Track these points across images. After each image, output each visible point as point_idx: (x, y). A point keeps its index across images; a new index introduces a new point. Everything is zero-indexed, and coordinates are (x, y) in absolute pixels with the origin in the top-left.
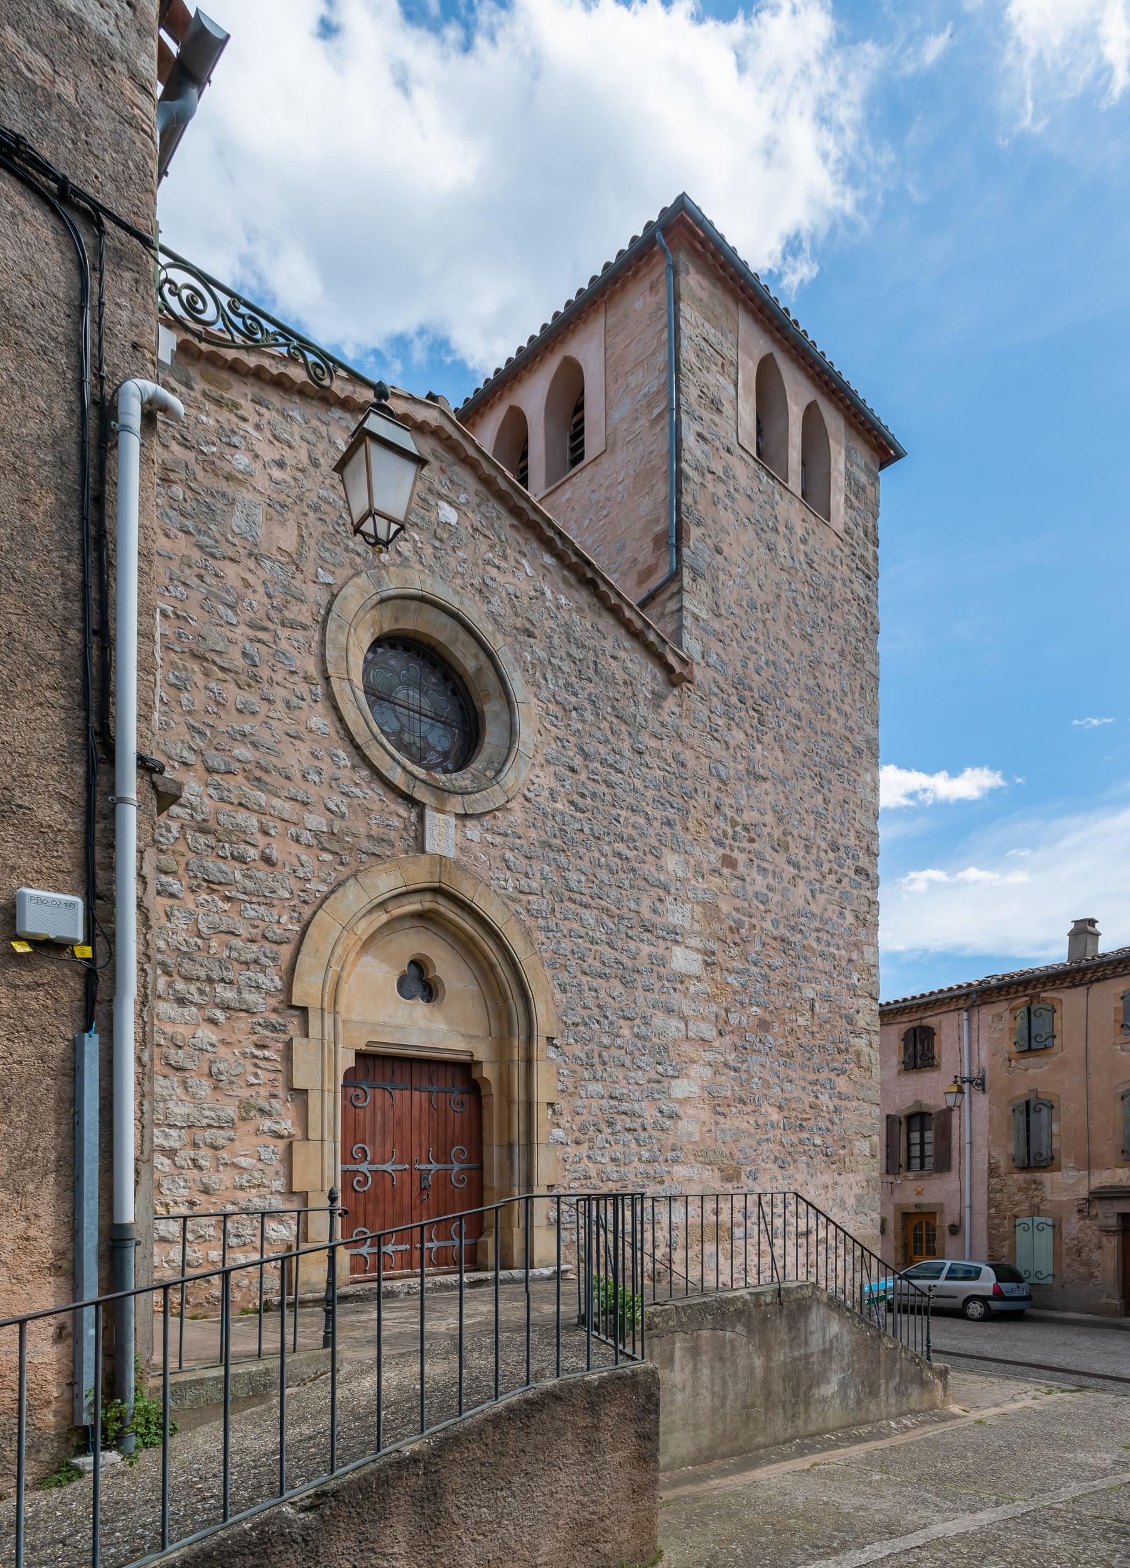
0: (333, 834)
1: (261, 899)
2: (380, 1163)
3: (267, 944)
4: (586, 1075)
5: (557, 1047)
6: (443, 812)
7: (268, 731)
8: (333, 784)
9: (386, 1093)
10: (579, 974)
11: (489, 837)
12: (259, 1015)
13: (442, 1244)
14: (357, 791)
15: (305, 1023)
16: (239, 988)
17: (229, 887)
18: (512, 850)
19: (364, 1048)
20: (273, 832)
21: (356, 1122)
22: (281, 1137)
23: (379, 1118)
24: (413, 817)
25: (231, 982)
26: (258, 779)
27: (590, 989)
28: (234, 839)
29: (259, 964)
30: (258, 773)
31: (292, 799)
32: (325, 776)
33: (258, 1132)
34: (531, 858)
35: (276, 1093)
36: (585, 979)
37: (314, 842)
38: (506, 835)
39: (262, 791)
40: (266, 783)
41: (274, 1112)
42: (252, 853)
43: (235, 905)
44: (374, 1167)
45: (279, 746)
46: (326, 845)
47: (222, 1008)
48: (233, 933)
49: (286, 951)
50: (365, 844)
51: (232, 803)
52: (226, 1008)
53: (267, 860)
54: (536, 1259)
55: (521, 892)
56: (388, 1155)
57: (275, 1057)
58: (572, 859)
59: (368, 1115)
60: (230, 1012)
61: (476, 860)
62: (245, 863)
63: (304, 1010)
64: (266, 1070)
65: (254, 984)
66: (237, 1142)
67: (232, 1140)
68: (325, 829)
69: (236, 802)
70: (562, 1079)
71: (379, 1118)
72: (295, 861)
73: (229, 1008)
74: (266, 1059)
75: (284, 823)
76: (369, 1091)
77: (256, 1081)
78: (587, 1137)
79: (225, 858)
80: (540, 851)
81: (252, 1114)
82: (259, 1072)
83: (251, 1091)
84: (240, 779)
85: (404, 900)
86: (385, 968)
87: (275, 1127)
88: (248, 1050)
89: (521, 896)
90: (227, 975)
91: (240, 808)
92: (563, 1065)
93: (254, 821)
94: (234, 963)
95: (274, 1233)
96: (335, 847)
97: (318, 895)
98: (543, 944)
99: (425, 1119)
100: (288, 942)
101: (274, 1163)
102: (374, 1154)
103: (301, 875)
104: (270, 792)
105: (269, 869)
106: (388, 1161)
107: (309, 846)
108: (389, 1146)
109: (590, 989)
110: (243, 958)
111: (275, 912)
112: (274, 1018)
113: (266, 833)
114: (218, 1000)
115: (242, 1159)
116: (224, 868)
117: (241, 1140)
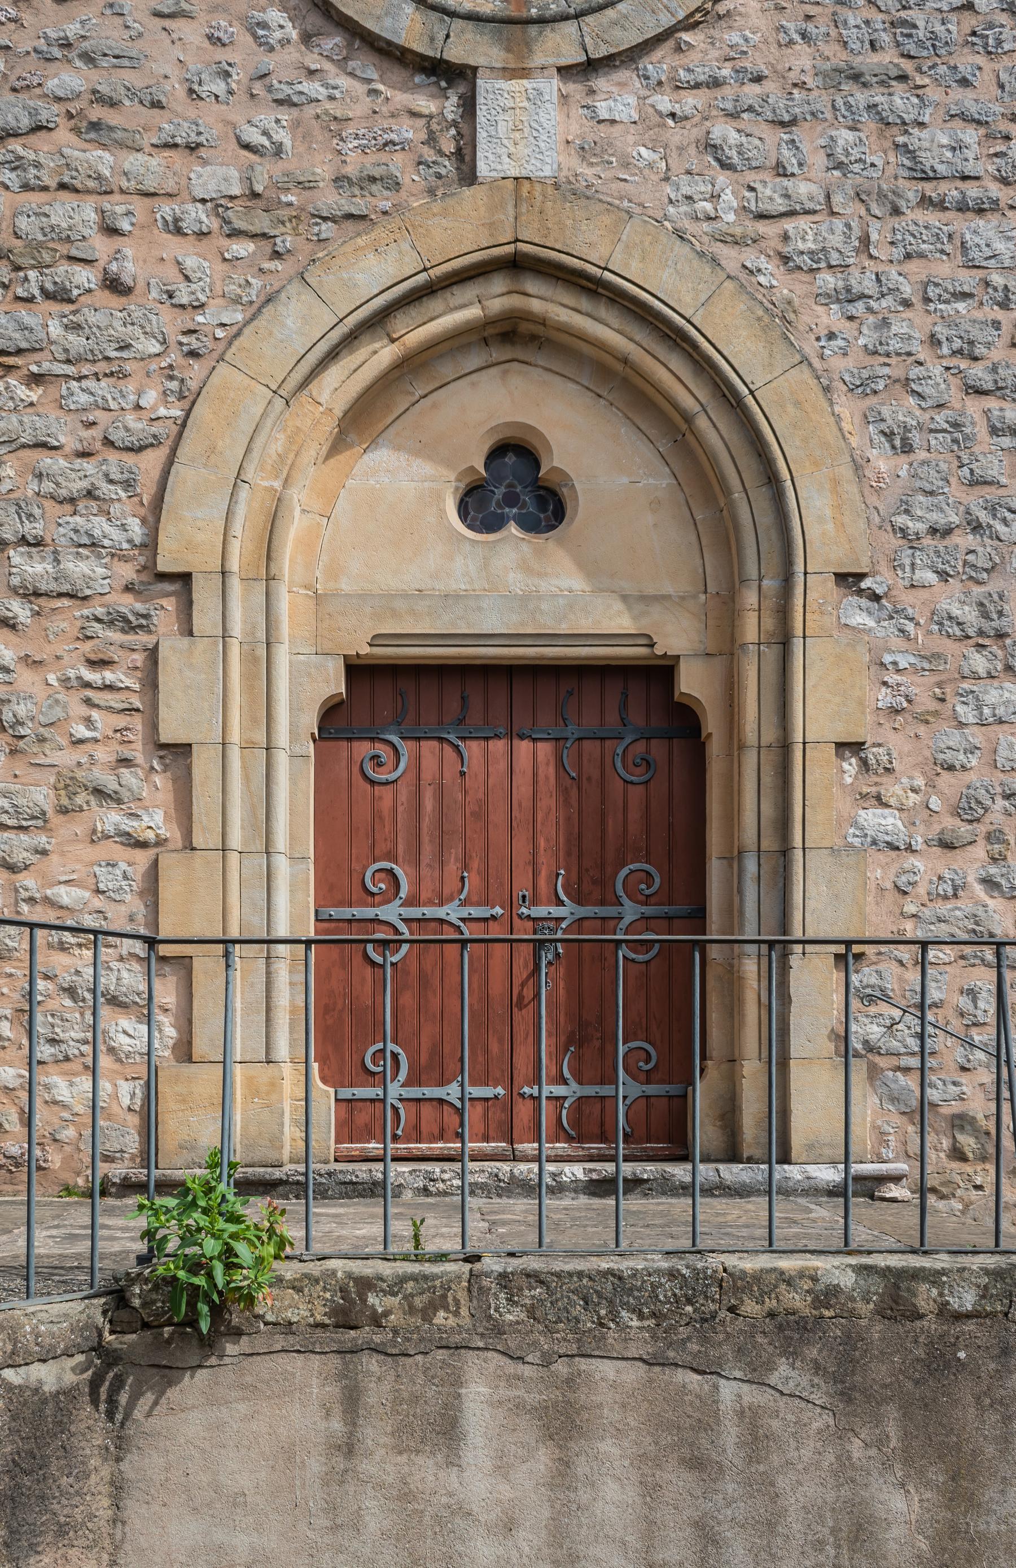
0: (255, 195)
1: (102, 367)
2: (430, 903)
3: (113, 457)
4: (979, 663)
5: (876, 598)
6: (523, 73)
7: (118, 21)
8: (258, 88)
9: (448, 749)
10: (954, 395)
11: (664, 102)
12: (97, 601)
13: (590, 1090)
14: (313, 88)
15: (187, 606)
16: (55, 552)
17: (37, 356)
18: (733, 115)
19: (365, 650)
20: (125, 225)
21: (376, 815)
22: (143, 845)
23: (429, 804)
24: (451, 106)
25: (39, 543)
26: (95, 126)
27: (994, 431)
28: (47, 257)
29: (97, 498)
30: (96, 113)
31: (167, 146)
32: (238, 75)
33: (95, 837)
34: (793, 122)
35: (127, 754)
36: (974, 407)
37: (215, 224)
38: (715, 83)
39: (104, 146)
40: (111, 129)
41: (125, 794)
42: (84, 277)
43: (52, 389)
44: (415, 912)
45: (139, 44)
46: (239, 224)
47: (25, 596)
48: (44, 445)
49: (151, 462)
50: (330, 200)
51: (45, 189)
52: (32, 594)
53: (114, 285)
54: (797, 1140)
55: (761, 216)
56: (451, 884)
57: (128, 682)
58: (934, 94)
59: (403, 797)
60: (42, 601)
61: (626, 165)
62: (71, 301)
63: (185, 578)
64: (109, 709)
65: (85, 540)
66: (54, 858)
67: (44, 853)
68: (236, 191)
69: (53, 184)
70: (892, 678)
71: (429, 804)
72: (171, 273)
73: (37, 594)
74: (110, 688)
75: (147, 201)
76: (405, 748)
77: (88, 734)
78: (982, 829)
79: (30, 300)
80: (821, 100)
81: (80, 800)
82: (95, 714)
83: (79, 755)
84: (63, 135)
85: (435, 304)
86: (423, 468)
87: (129, 825)
88: (72, 673)
89: (762, 227)
90: (34, 529)
91: (64, 195)
92: (897, 642)
93: (88, 212)
94: (48, 504)
95: (127, 1040)
96: (261, 223)
97: (220, 333)
98: (831, 336)
99: (548, 802)
100: (155, 442)
101: (128, 898)
102: (417, 882)
103: (185, 301)
104: (122, 145)
105: (115, 301)
106: (451, 899)
107: (201, 235)
108: (453, 867)
109: (994, 431)
110: (64, 492)
111: (130, 387)
112: (127, 604)
113: (112, 231)
114: (15, 581)
115: (62, 890)
116: (29, 320)
117: (62, 854)
